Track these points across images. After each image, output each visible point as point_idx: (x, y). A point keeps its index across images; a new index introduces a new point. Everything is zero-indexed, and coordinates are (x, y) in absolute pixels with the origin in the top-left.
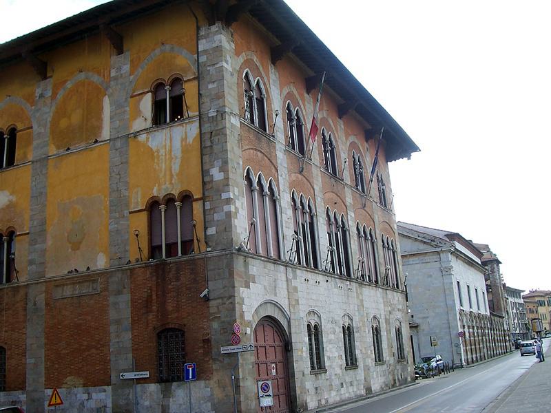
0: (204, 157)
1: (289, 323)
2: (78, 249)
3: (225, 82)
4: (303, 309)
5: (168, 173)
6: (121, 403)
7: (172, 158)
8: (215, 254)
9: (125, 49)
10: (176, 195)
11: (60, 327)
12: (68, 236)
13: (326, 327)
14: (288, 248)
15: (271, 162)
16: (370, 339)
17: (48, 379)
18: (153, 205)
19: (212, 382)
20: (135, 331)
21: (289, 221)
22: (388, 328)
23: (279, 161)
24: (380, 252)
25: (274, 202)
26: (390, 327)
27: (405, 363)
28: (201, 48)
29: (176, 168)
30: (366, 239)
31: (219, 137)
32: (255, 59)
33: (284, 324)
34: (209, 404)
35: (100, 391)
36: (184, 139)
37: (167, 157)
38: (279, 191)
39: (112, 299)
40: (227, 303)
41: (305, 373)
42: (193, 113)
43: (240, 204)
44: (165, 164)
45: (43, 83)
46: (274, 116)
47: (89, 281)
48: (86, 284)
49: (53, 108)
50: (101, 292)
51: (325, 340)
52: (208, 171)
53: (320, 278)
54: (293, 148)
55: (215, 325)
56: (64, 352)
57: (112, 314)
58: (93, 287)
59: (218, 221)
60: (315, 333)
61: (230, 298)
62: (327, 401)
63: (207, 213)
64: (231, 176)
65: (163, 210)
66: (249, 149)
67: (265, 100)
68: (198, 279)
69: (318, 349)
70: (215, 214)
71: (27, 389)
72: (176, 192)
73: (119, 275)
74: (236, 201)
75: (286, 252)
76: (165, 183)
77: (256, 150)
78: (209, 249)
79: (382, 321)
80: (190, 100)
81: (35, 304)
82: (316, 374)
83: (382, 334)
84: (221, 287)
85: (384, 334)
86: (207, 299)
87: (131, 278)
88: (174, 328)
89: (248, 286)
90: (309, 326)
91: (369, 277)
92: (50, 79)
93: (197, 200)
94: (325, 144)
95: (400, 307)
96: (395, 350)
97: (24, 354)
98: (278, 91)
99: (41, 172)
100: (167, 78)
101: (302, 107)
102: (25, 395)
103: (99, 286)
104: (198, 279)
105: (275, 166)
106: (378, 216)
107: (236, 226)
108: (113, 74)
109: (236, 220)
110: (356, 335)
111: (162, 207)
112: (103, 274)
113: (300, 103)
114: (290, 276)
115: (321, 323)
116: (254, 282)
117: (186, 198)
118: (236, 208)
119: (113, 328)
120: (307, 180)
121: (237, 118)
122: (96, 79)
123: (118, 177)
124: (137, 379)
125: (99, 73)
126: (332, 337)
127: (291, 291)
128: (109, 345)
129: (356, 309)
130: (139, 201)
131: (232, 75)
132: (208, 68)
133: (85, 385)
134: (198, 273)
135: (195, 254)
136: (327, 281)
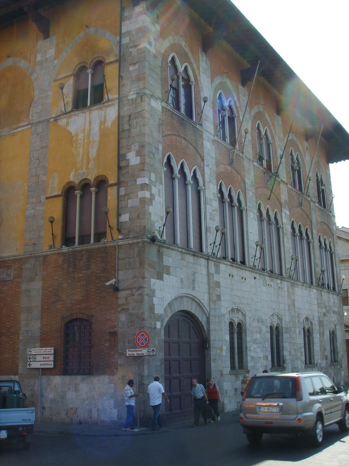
1: (208, 319)
4: (225, 307)
5: (85, 157)
8: (126, 242)
9: (51, 34)
10: (92, 180)
13: (251, 325)
14: (211, 240)
16: (300, 341)
18: (69, 191)
19: (116, 377)
22: (322, 331)
23: (206, 151)
24: (316, 252)
25: (309, 243)
26: (324, 329)
27: (339, 367)
28: (124, 30)
29: (93, 152)
31: (137, 120)
33: (202, 319)
34: (112, 402)
36: (102, 123)
37: (86, 141)
38: (204, 181)
39: (24, 286)
40: (136, 294)
41: (224, 373)
42: (113, 96)
46: (203, 103)
51: (248, 339)
52: (124, 155)
53: (247, 274)
55: (123, 317)
58: (7, 273)
59: (132, 207)
60: (237, 331)
61: (139, 288)
65: (78, 196)
66: (172, 135)
67: (193, 87)
70: (129, 201)
72: (92, 178)
74: (153, 187)
75: (209, 245)
76: (82, 169)
77: (179, 136)
78: (121, 237)
79: (316, 322)
80: (111, 83)
83: (314, 335)
85: (316, 337)
86: (116, 289)
88: (82, 319)
89: (160, 277)
91: (328, 285)
93: (112, 185)
94: (260, 138)
95: (336, 309)
96: (328, 353)
98: (209, 80)
100: (90, 61)
105: (201, 156)
106: (316, 217)
109: (150, 207)
110: (285, 336)
111: (78, 193)
112: (17, 260)
113: (234, 94)
114: (212, 270)
116: (168, 273)
117: (101, 183)
118: (151, 194)
123: (37, 161)
124: (43, 369)
126: (258, 336)
129: (287, 308)
130: (56, 187)
132: (130, 50)
135: (107, 242)
136: (255, 278)
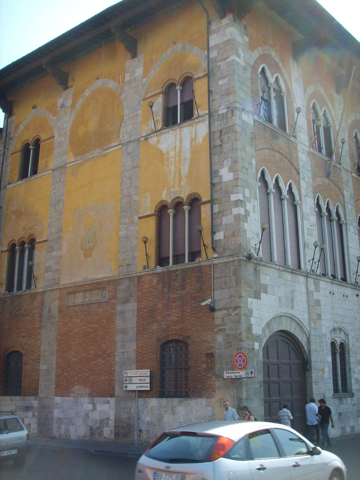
0: (213, 157)
1: (308, 339)
2: (90, 256)
3: (236, 77)
5: (177, 175)
6: (124, 417)
7: (181, 160)
8: (221, 261)
10: (185, 198)
11: (70, 334)
12: (81, 243)
15: (292, 164)
17: (58, 386)
18: (161, 211)
19: (213, 400)
20: (140, 341)
21: (312, 228)
23: (301, 164)
28: (212, 44)
29: (185, 169)
30: (330, 220)
31: (229, 135)
32: (273, 54)
33: (302, 339)
35: (104, 403)
36: (193, 140)
37: (177, 159)
38: (300, 195)
39: (119, 308)
40: (233, 314)
43: (252, 207)
44: (175, 166)
45: (64, 93)
47: (99, 288)
48: (96, 291)
49: (73, 117)
50: (109, 299)
51: (352, 360)
52: (217, 172)
54: (320, 150)
55: (220, 338)
56: (73, 359)
57: (119, 324)
58: (102, 295)
59: (226, 225)
62: (353, 428)
63: (215, 217)
64: (241, 176)
65: (171, 214)
66: (265, 148)
67: (285, 98)
68: (203, 287)
69: (344, 370)
70: (224, 218)
71: (40, 395)
73: (127, 282)
75: (307, 261)
76: (174, 187)
77: (272, 149)
78: (216, 255)
81: (50, 311)
82: (340, 399)
84: (228, 297)
87: (138, 285)
89: (257, 296)
90: (333, 344)
92: (71, 89)
93: (205, 203)
97: (37, 361)
99: (60, 180)
100: (177, 77)
101: (331, 107)
102: (37, 402)
103: (107, 294)
104: (203, 287)
105: (296, 169)
107: (245, 231)
108: (127, 78)
109: (245, 224)
111: (171, 212)
114: (312, 287)
115: (348, 341)
116: (266, 292)
117: (195, 201)
118: (246, 211)
119: (118, 338)
120: (335, 184)
121: (251, 115)
122: (112, 85)
123: (129, 181)
124: (139, 391)
125: (114, 79)
127: (313, 304)
128: (114, 356)
130: (148, 206)
131: (245, 69)
132: (219, 64)
133: (91, 395)
134: (202, 280)
